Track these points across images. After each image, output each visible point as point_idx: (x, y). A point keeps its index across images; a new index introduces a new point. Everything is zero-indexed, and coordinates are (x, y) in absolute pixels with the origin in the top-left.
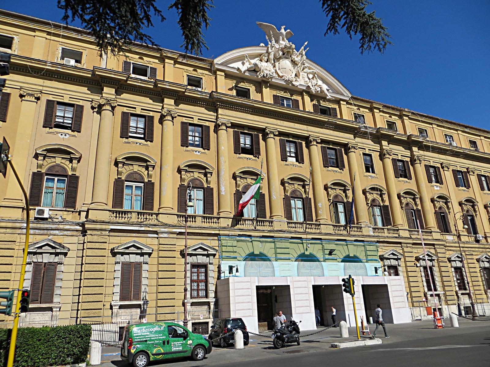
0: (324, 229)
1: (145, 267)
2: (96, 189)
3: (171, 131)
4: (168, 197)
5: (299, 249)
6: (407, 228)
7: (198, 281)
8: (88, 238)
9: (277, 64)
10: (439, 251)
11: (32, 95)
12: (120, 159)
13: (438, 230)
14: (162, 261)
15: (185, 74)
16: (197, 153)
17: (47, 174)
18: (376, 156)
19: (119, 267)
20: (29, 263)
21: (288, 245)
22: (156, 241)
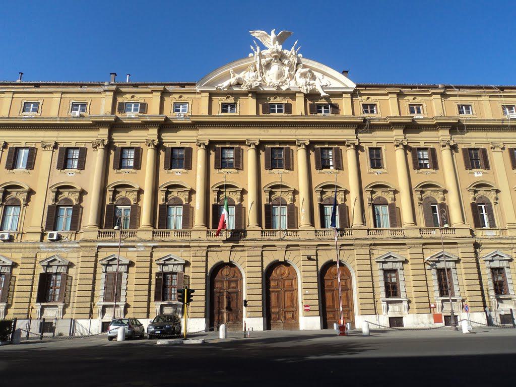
0: (302, 235)
3: (46, 159)
16: (178, 174)
22: (136, 254)
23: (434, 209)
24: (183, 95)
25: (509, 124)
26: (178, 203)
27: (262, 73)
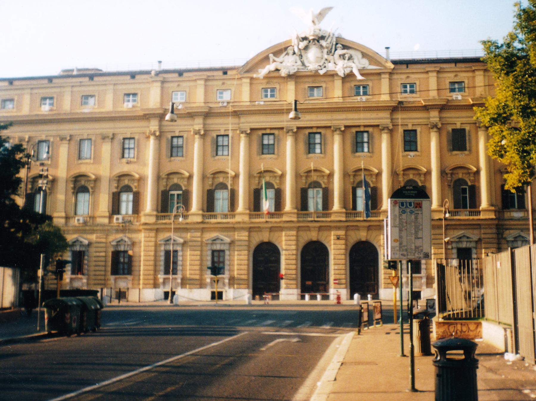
23: (464, 191)
24: (181, 84)
25: (362, 105)
26: (223, 186)
27: (301, 56)
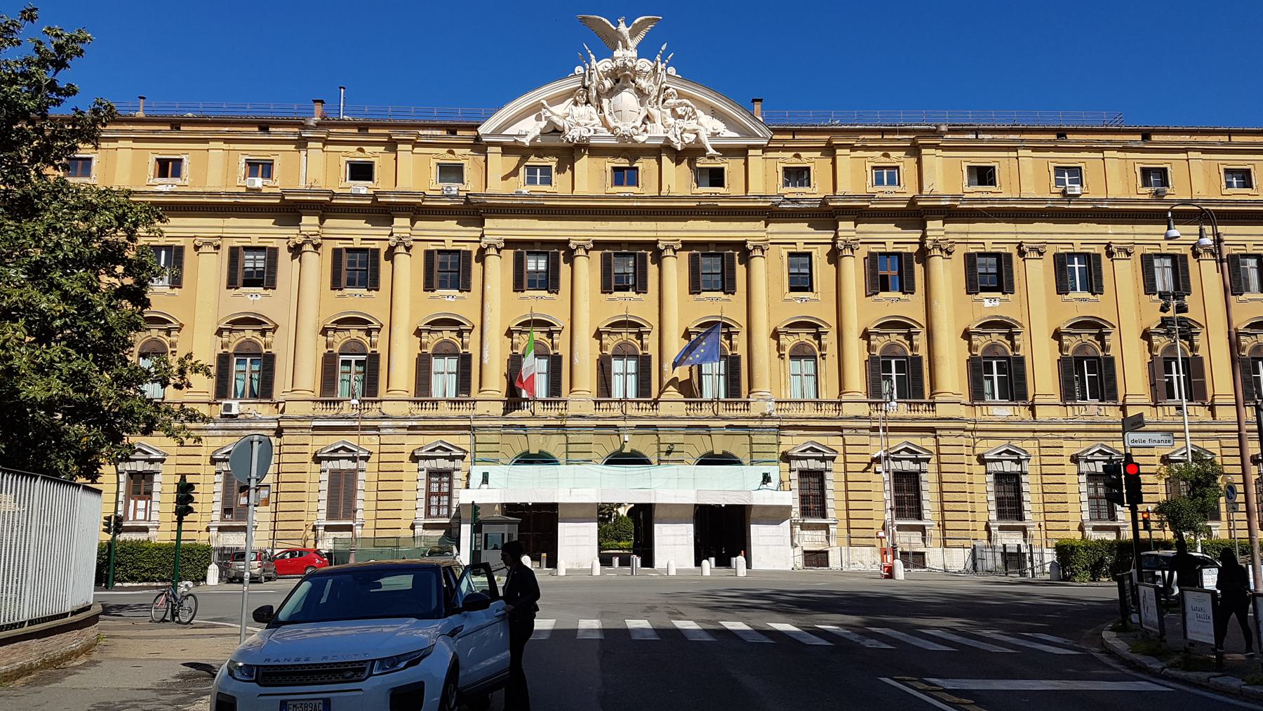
1: (361, 476)
2: (299, 374)
4: (401, 375)
5: (612, 445)
6: (865, 398)
7: (439, 494)
8: (285, 439)
9: (605, 101)
10: (849, 440)
11: (210, 244)
12: (602, 327)
13: (681, 397)
14: (383, 467)
15: (433, 163)
17: (236, 355)
18: (820, 255)
19: (325, 476)
20: (219, 473)
21: (495, 438)
